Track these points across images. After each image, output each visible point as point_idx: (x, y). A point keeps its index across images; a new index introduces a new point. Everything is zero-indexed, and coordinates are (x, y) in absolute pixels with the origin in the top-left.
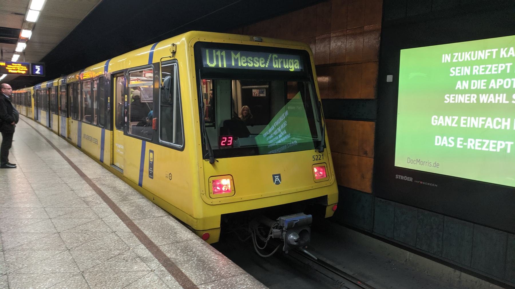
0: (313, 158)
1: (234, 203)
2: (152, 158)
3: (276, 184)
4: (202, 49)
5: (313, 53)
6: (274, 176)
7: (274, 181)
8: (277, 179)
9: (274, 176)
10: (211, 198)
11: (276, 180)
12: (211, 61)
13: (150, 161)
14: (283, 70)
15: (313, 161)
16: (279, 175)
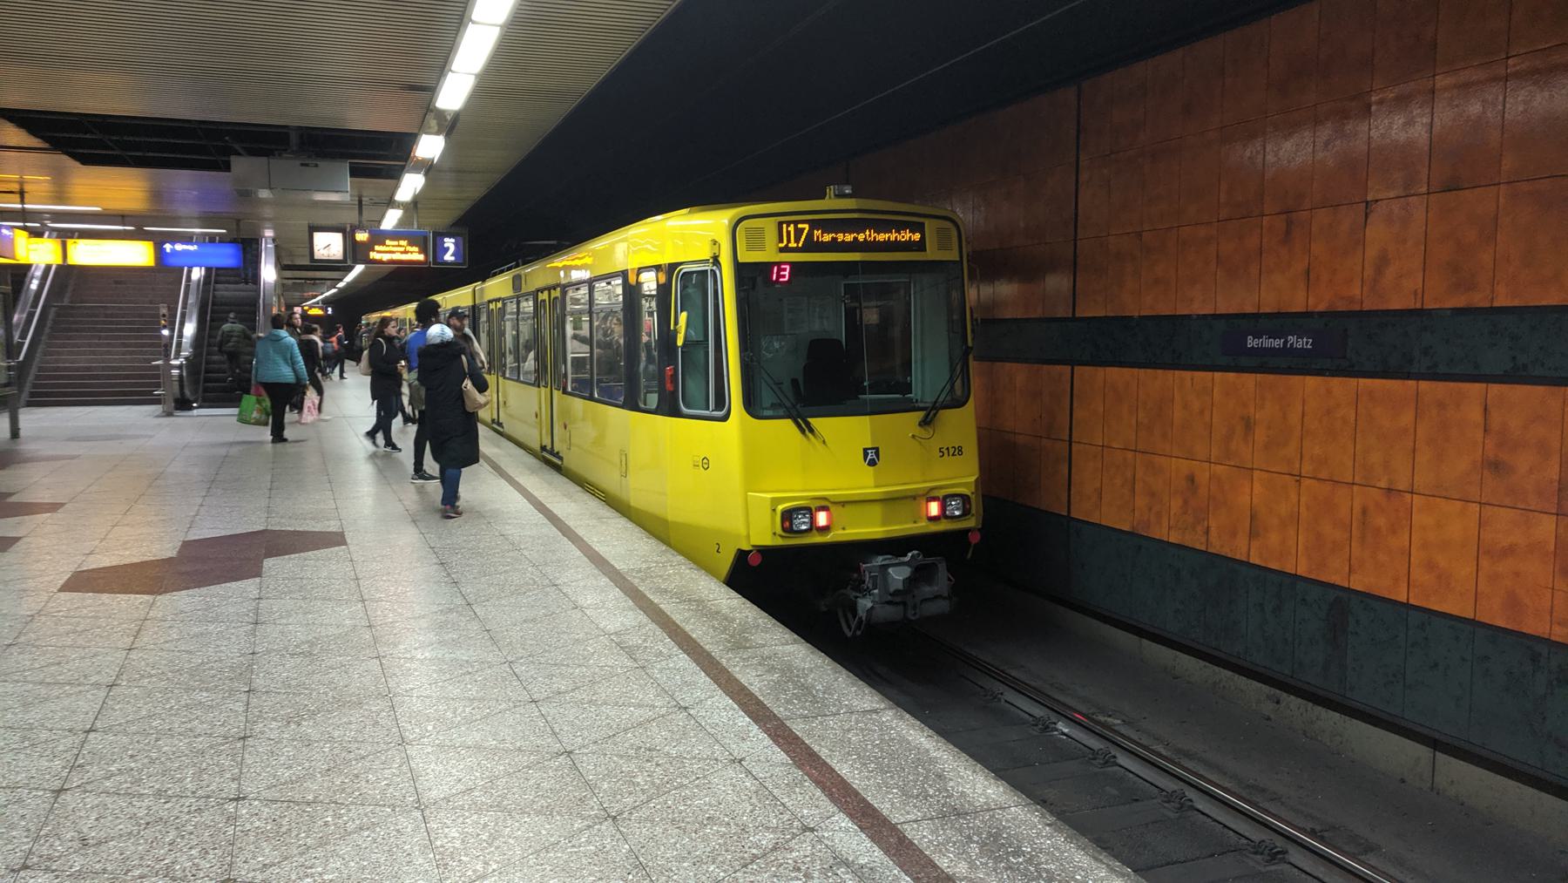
3: (869, 464)
5: (587, 288)
7: (865, 461)
9: (865, 450)
11: (869, 457)
16: (877, 450)
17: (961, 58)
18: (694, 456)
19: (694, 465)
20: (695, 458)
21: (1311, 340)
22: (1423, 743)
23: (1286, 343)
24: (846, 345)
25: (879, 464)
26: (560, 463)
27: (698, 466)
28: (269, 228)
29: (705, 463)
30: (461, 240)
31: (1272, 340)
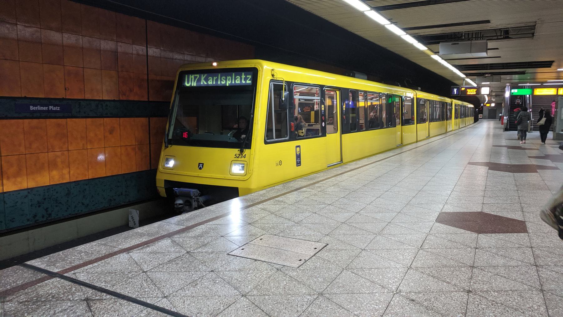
0: (235, 155)
1: (200, 178)
2: (299, 151)
4: (252, 73)
6: (199, 164)
7: (198, 167)
8: (201, 166)
10: (246, 175)
11: (200, 167)
12: (188, 83)
13: (297, 154)
14: (221, 85)
15: (235, 158)
16: (203, 164)
17: (126, 5)
18: (276, 161)
19: (277, 165)
20: (277, 162)
21: (59, 108)
22: (294, 191)
23: (48, 108)
24: (167, 121)
25: (202, 169)
26: (531, 95)
27: (278, 165)
28: (217, 64)
29: (280, 163)
30: (251, 84)
31: (42, 107)
